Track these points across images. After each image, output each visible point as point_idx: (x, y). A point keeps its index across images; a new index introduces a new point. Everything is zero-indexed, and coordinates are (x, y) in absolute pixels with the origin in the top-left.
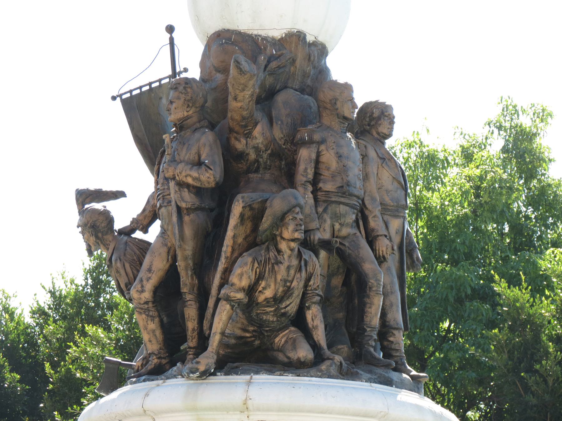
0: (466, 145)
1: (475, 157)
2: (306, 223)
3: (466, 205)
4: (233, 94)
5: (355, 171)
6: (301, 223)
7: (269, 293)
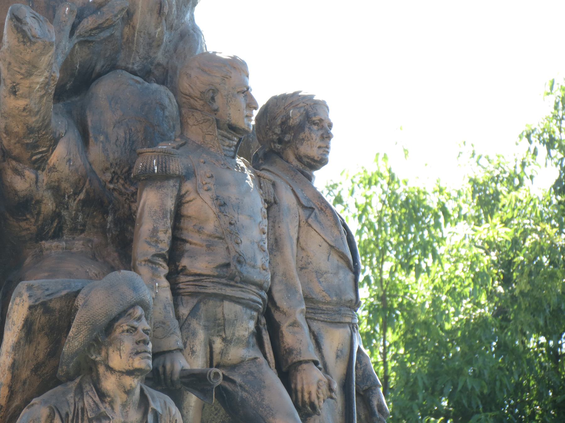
0: (482, 177)
1: (503, 201)
2: (155, 339)
3: (483, 299)
4: (8, 82)
5: (253, 234)
6: (147, 337)
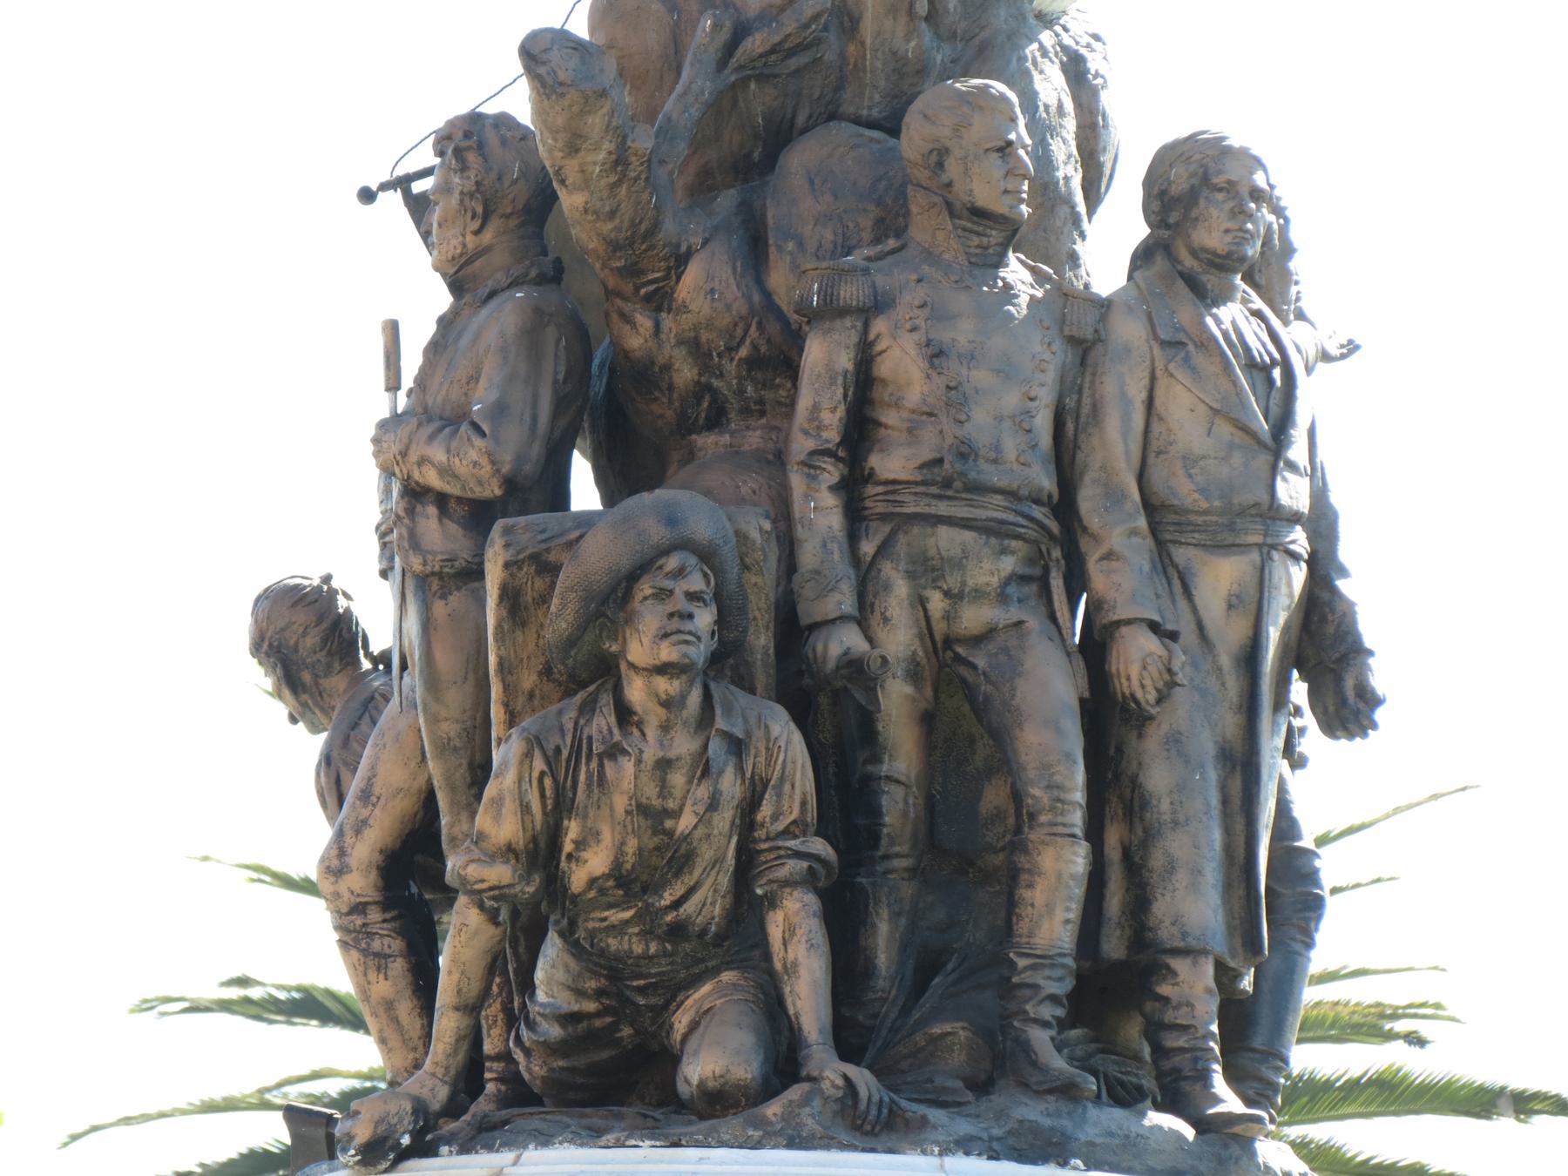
7: (597, 862)
